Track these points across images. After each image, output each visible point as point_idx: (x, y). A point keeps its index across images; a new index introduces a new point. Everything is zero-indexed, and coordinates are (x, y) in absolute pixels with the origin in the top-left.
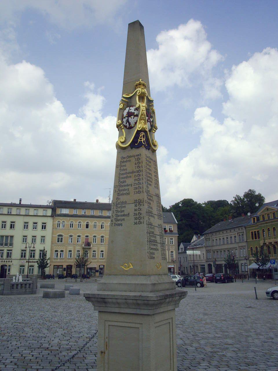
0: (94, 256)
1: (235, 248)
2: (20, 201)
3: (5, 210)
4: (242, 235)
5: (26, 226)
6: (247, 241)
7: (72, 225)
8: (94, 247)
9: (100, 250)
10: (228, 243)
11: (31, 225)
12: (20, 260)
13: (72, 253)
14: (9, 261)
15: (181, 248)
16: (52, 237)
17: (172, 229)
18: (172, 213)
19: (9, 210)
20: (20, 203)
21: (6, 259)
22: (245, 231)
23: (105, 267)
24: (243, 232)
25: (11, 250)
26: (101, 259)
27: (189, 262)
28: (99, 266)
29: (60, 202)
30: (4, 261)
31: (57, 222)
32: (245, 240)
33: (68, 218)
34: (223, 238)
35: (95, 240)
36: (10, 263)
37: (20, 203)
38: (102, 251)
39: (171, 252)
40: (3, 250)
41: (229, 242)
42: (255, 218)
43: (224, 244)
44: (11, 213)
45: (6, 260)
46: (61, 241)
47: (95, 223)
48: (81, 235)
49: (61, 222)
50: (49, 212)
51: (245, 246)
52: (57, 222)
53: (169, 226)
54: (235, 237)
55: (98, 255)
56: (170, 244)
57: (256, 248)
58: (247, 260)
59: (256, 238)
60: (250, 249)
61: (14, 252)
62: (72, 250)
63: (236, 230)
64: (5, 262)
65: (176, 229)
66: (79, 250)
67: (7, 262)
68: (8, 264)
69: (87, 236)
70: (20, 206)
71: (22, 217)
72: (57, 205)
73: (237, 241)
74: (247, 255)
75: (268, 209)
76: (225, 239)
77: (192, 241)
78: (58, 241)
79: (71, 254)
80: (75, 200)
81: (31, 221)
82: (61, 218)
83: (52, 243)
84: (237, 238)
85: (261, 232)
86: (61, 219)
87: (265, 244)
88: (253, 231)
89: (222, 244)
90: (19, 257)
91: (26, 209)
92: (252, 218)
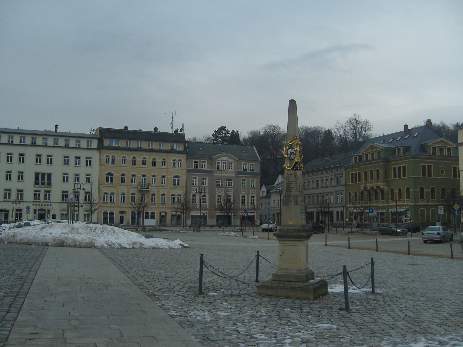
0: (153, 199)
1: (331, 193)
2: (56, 127)
3: (5, 139)
4: (341, 177)
5: (66, 160)
6: (345, 185)
7: (124, 162)
8: (153, 190)
9: (161, 193)
10: (322, 187)
11: (72, 161)
12: (62, 204)
13: (166, 197)
14: (48, 205)
15: (263, 192)
16: (100, 176)
17: (254, 168)
18: (254, 148)
19: (55, 141)
20: (56, 131)
21: (44, 202)
22: (344, 173)
23: (167, 214)
24: (342, 174)
25: (49, 191)
26: (162, 204)
27: (273, 209)
28: (160, 213)
29: (108, 130)
30: (42, 205)
31: (161, 159)
32: (344, 183)
33: (119, 152)
34: (318, 181)
35: (154, 181)
36: (50, 208)
37: (56, 131)
38: (163, 195)
39: (242, 197)
40: (39, 191)
41: (325, 186)
42: (358, 157)
43: (318, 188)
44: (57, 144)
45: (44, 204)
46: (111, 181)
47: (124, 157)
48: (136, 174)
49: (111, 156)
50: (95, 144)
51: (343, 190)
52: (105, 157)
53: (250, 165)
54: (332, 179)
55: (158, 199)
56: (202, 186)
57: (356, 193)
58: (343, 207)
59: (356, 181)
60: (348, 195)
61: (52, 194)
62: (126, 192)
63: (333, 171)
64: (43, 206)
65: (259, 168)
66: (134, 192)
67: (45, 205)
68: (47, 208)
69: (144, 176)
70: (56, 135)
71: (61, 149)
72: (105, 134)
73: (334, 184)
74: (344, 201)
75: (372, 147)
76: (320, 181)
77: (277, 183)
78: (175, 184)
79: (164, 198)
80: (126, 128)
81: (72, 154)
82: (177, 155)
83: (100, 183)
84: (334, 180)
85: (363, 175)
86: (111, 154)
87: (366, 189)
88: (357, 172)
89: (311, 188)
90: (60, 200)
91: (43, 138)
92: (354, 157)
